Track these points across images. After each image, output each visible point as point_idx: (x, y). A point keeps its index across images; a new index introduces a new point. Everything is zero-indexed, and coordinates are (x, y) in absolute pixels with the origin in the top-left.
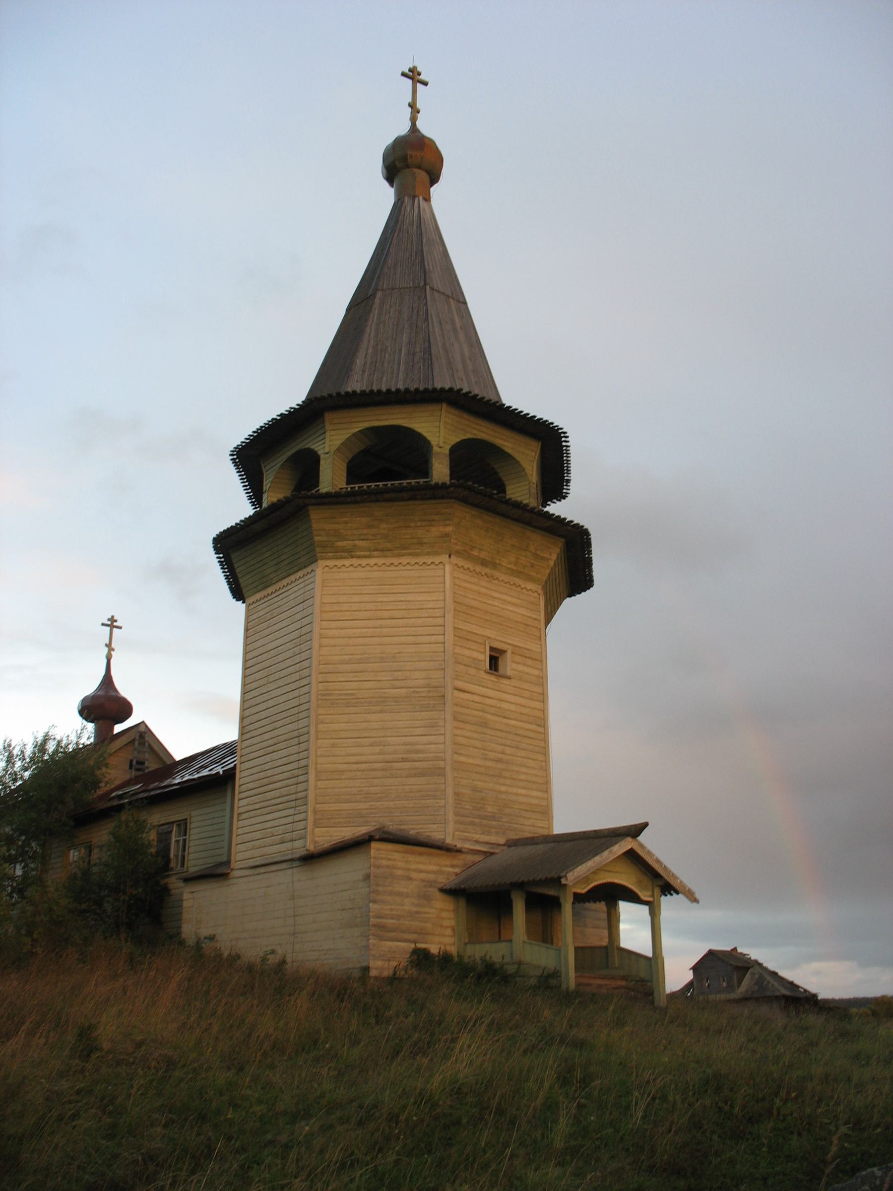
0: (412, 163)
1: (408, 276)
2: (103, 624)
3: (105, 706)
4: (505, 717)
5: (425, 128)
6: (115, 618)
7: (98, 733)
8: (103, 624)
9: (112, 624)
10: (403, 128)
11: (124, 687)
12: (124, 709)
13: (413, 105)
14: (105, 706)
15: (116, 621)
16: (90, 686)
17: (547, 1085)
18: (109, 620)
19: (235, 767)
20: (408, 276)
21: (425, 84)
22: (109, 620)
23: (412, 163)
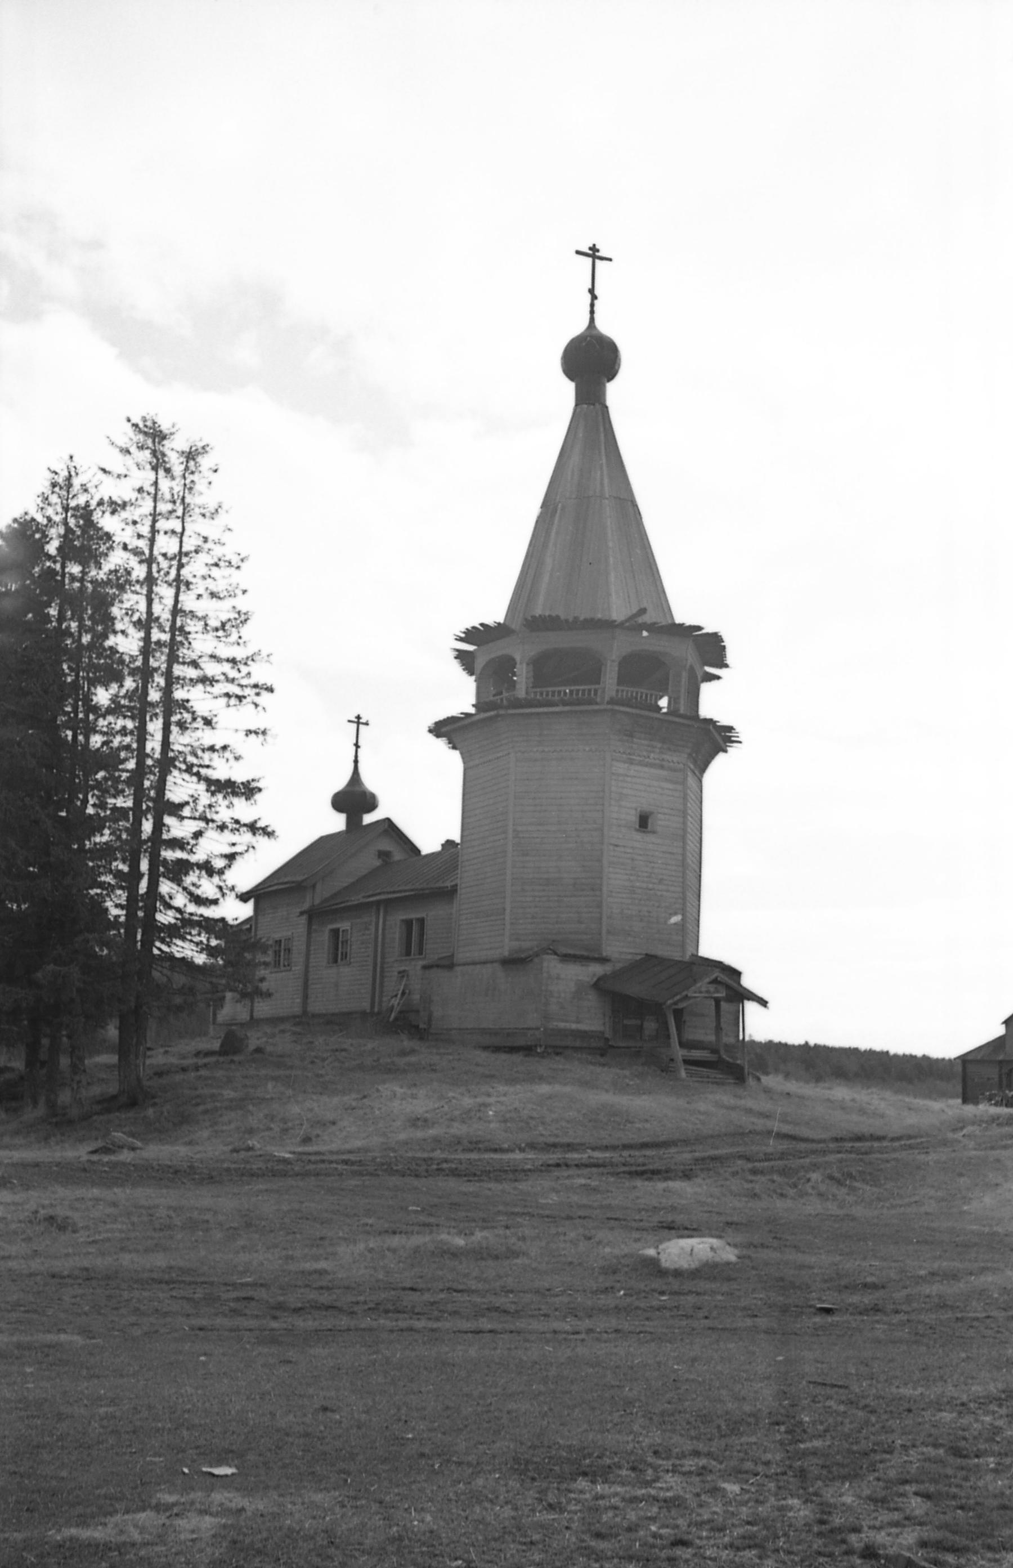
0: (591, 362)
1: (589, 497)
2: (349, 721)
3: (354, 800)
4: (495, 1151)
5: (605, 327)
6: (597, 247)
7: (349, 822)
8: (349, 721)
9: (358, 721)
10: (578, 327)
11: (370, 782)
12: (370, 803)
13: (592, 291)
14: (354, 800)
15: (598, 251)
16: (340, 781)
17: (648, 1126)
18: (590, 249)
19: (456, 885)
20: (589, 497)
21: (367, 724)
22: (590, 249)
23: (591, 362)
